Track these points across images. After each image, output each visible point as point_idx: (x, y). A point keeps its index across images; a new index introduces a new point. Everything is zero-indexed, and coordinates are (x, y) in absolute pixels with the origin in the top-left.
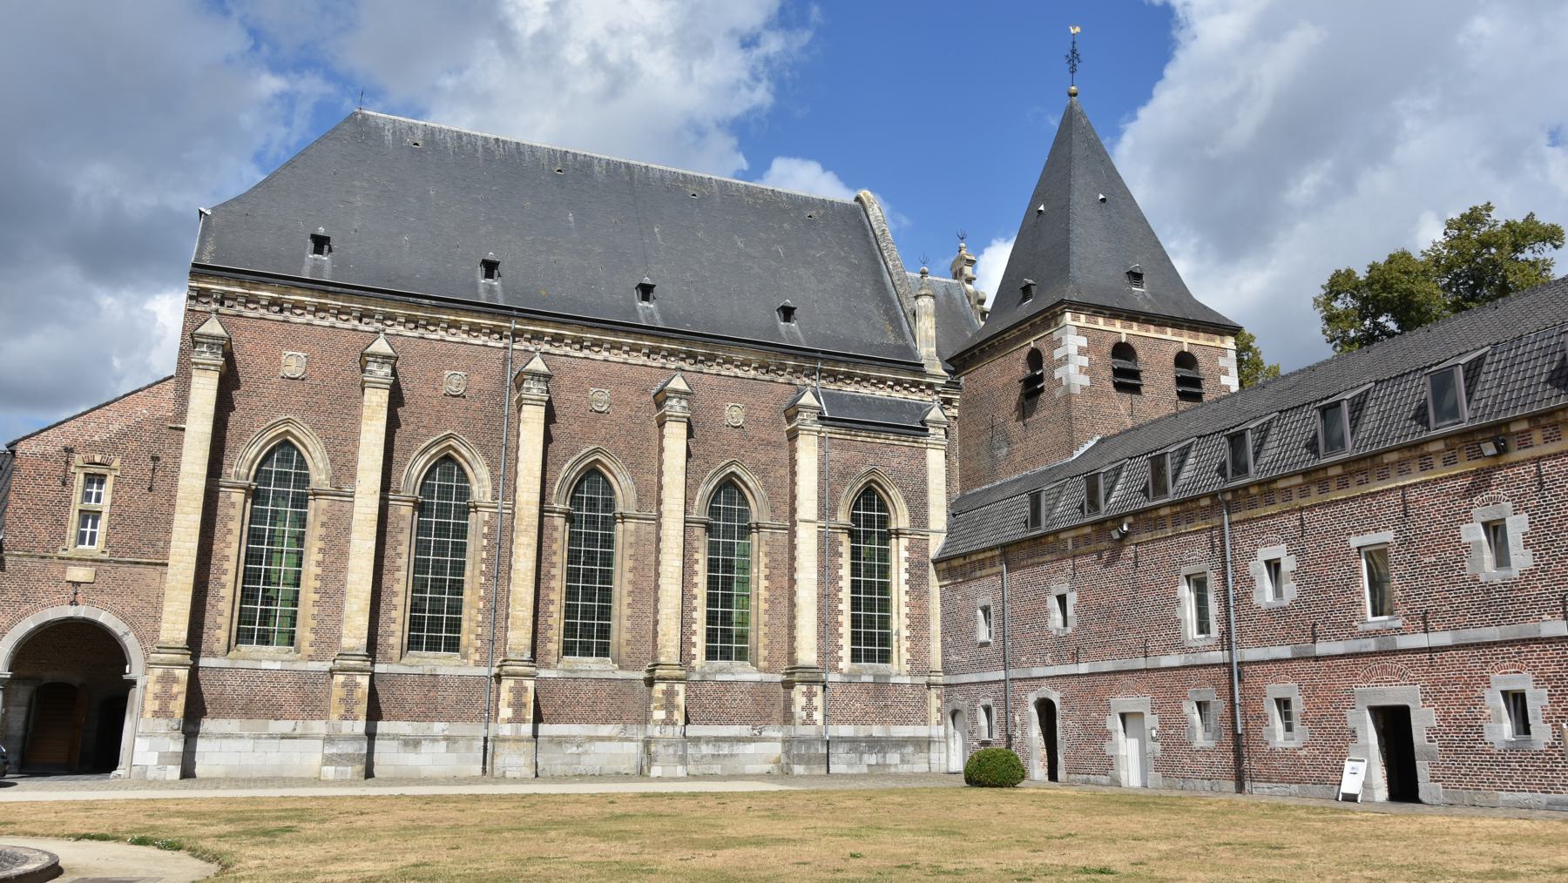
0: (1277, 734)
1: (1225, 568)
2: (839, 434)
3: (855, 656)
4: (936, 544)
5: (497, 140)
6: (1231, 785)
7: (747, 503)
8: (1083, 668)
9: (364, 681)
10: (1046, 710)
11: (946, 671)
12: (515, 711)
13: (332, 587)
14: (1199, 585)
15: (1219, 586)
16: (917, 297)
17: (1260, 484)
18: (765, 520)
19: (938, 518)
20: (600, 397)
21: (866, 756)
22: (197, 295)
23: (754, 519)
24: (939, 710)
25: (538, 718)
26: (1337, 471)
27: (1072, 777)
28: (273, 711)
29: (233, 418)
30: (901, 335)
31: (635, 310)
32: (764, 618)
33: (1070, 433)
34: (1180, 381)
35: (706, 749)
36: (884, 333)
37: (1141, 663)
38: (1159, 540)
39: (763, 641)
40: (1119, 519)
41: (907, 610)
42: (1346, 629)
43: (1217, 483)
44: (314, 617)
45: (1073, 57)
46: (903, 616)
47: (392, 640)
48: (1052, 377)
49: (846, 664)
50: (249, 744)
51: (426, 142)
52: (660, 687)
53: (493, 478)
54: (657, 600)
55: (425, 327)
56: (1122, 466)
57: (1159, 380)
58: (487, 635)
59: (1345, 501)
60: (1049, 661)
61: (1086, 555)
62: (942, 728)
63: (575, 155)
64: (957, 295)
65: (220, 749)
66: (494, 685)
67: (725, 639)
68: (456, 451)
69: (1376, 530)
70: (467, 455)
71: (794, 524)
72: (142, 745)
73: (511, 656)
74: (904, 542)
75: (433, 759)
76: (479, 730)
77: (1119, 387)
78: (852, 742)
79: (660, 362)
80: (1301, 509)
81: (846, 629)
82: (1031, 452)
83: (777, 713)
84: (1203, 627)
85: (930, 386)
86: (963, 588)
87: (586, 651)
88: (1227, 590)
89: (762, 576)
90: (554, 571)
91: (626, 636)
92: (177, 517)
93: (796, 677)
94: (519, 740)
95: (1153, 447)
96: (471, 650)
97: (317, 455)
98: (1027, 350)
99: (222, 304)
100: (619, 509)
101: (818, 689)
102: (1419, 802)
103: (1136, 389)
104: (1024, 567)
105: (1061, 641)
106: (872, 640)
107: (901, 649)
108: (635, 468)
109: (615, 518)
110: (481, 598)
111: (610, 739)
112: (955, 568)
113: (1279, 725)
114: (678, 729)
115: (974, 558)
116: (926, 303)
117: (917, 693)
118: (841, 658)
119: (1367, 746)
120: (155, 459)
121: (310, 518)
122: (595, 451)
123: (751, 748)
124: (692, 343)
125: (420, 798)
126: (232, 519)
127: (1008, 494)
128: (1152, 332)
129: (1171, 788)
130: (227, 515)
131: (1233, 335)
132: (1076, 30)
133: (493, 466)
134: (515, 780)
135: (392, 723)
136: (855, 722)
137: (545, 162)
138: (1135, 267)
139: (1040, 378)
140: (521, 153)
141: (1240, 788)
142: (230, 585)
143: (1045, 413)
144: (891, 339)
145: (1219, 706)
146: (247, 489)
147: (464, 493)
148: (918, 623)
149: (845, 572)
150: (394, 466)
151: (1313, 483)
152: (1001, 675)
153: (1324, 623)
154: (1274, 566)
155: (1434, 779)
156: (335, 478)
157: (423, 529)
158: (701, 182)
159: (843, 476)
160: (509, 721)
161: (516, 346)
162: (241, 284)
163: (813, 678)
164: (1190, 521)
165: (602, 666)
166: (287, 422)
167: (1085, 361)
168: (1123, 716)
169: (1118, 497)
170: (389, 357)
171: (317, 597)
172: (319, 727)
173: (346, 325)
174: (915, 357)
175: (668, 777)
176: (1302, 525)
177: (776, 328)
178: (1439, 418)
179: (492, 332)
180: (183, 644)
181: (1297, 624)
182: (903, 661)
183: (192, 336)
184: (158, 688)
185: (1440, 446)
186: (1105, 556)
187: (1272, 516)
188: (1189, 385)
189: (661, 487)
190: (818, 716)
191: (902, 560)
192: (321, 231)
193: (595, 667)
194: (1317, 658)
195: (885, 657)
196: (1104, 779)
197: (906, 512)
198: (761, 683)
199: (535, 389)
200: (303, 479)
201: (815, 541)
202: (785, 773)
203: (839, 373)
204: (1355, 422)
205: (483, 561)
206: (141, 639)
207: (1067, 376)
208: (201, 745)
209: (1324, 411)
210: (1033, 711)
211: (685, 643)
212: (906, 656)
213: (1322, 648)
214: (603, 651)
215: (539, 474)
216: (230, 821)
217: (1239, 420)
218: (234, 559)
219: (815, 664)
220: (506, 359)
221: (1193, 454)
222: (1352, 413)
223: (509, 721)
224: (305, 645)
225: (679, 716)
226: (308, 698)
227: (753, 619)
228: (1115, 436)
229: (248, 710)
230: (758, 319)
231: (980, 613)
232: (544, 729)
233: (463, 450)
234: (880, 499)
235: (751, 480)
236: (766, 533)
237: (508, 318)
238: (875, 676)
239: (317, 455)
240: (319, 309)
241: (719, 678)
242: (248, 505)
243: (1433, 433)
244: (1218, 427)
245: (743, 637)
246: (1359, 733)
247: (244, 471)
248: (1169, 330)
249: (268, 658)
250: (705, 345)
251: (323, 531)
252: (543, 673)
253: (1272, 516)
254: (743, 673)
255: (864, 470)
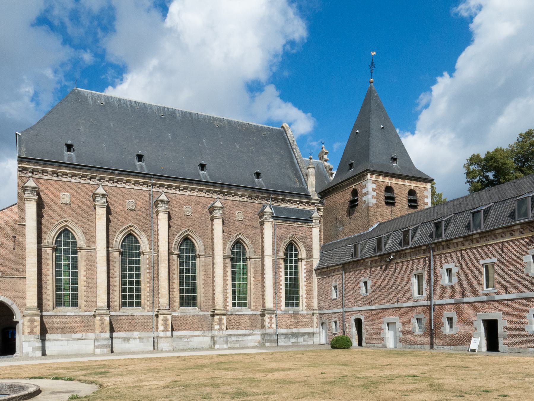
0: (447, 329)
1: (430, 271)
2: (279, 223)
3: (287, 305)
4: (316, 264)
5: (135, 102)
6: (428, 347)
7: (245, 249)
8: (373, 307)
9: (107, 318)
10: (359, 322)
11: (319, 309)
12: (165, 327)
13: (91, 284)
14: (419, 277)
15: (427, 278)
16: (308, 168)
17: (446, 241)
18: (252, 256)
19: (316, 253)
20: (188, 210)
21: (291, 339)
22: (22, 170)
23: (248, 255)
24: (317, 323)
25: (173, 330)
26: (478, 236)
27: (368, 345)
28: (73, 330)
29: (44, 220)
30: (301, 183)
31: (199, 175)
32: (253, 291)
33: (368, 221)
34: (410, 201)
35: (234, 339)
36: (295, 183)
37: (396, 305)
38: (405, 261)
39: (253, 300)
40: (389, 254)
41: (305, 288)
42: (476, 293)
43: (429, 241)
44: (85, 296)
45: (372, 66)
46: (304, 290)
47: (115, 303)
48: (361, 200)
49: (283, 307)
50: (65, 343)
51: (106, 103)
52: (217, 318)
53: (149, 242)
54: (214, 286)
55: (117, 182)
56: (390, 234)
57: (402, 200)
58: (151, 301)
59: (479, 247)
60: (360, 305)
61: (376, 267)
62: (318, 329)
63: (168, 109)
64: (321, 167)
65: (56, 344)
66: (155, 318)
67: (239, 299)
68: (133, 231)
69: (490, 258)
70: (138, 233)
71: (263, 257)
72: (25, 345)
73: (161, 308)
74: (304, 263)
75: (135, 345)
76: (151, 335)
77: (387, 203)
78: (286, 334)
79: (210, 195)
80: (462, 250)
81: (283, 295)
82: (352, 228)
83: (259, 325)
84: (420, 292)
85: (313, 203)
86: (327, 279)
87: (188, 305)
88: (430, 279)
89: (252, 276)
90: (174, 276)
91: (202, 299)
92: (27, 259)
93: (266, 312)
94: (167, 337)
95: (402, 227)
96: (146, 306)
97: (79, 234)
98: (351, 189)
99: (33, 173)
100: (198, 252)
101: (274, 316)
102: (498, 351)
103: (393, 204)
104: (351, 272)
105: (365, 298)
106: (292, 299)
107: (303, 301)
108: (203, 236)
109: (196, 256)
110: (148, 287)
111: (199, 336)
112: (323, 272)
113: (447, 326)
114: (224, 332)
115: (331, 268)
116: (312, 171)
117: (309, 317)
118: (281, 305)
119: (481, 333)
120: (14, 237)
121: (79, 258)
122: (187, 231)
123: (250, 338)
124: (222, 188)
125: (143, 359)
126: (48, 260)
127: (344, 245)
128: (400, 182)
129: (405, 348)
130: (46, 258)
131: (430, 182)
132: (373, 53)
133: (149, 237)
134: (166, 352)
135: (119, 333)
136: (287, 327)
137: (156, 111)
138: (394, 155)
139: (357, 200)
140: (146, 108)
141: (432, 347)
142: (51, 285)
143: (359, 214)
144: (298, 185)
145: (425, 320)
146: (53, 248)
147: (138, 248)
148: (309, 292)
149: (283, 274)
150: (110, 238)
151: (467, 240)
152: (341, 310)
153: (467, 291)
154: (449, 271)
155: (504, 344)
156: (88, 243)
157: (123, 261)
158: (220, 120)
159: (281, 238)
160: (163, 331)
161: (154, 190)
162: (40, 165)
163: (272, 313)
164: (417, 255)
165: (195, 310)
166: (66, 221)
167: (374, 194)
168: (388, 324)
169: (389, 246)
170: (105, 195)
171: (85, 288)
172: (91, 335)
173: (85, 182)
174: (307, 192)
175: (221, 349)
176: (462, 256)
177: (254, 182)
178: (519, 216)
179: (144, 184)
180: (36, 307)
181: (458, 291)
182: (304, 306)
183: (23, 187)
184: (29, 324)
185: (519, 227)
186: (383, 267)
187: (450, 253)
188: (413, 203)
189: (213, 244)
190: (274, 326)
191: (303, 269)
192: (69, 142)
193: (192, 311)
194: (464, 303)
195: (297, 304)
196: (380, 345)
197: (305, 252)
198: (253, 315)
199: (163, 207)
200: (75, 244)
201: (272, 263)
202: (262, 346)
203: (279, 199)
204: (485, 218)
205: (147, 273)
206: (18, 306)
207: (368, 199)
208: (47, 344)
209: (473, 214)
210: (353, 322)
211: (225, 301)
212: (305, 304)
213: (466, 300)
214: (194, 305)
215: (167, 240)
216: (82, 370)
217: (438, 217)
218: (51, 275)
219: (272, 308)
220: (150, 195)
221: (419, 230)
222: (484, 214)
223: (163, 331)
224: (83, 306)
225: (224, 327)
226: (87, 325)
227: (249, 292)
228: (385, 222)
229: (64, 330)
230: (244, 176)
231: (333, 288)
232: (175, 333)
233: (136, 231)
234: (295, 247)
235: (247, 241)
236: (253, 260)
237: (150, 178)
238: (294, 311)
239: (79, 234)
240: (73, 175)
241: (237, 313)
242: (54, 254)
243: (516, 222)
244: (429, 219)
245: (245, 298)
246: (478, 329)
247: (51, 241)
248: (406, 181)
249: (69, 311)
250: (227, 189)
251: (85, 263)
252: (174, 314)
253: (450, 253)
254: (246, 311)
255: (289, 236)
